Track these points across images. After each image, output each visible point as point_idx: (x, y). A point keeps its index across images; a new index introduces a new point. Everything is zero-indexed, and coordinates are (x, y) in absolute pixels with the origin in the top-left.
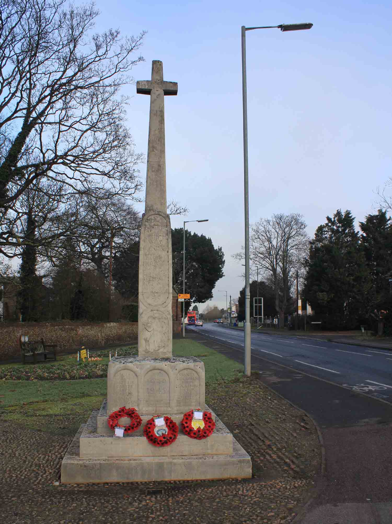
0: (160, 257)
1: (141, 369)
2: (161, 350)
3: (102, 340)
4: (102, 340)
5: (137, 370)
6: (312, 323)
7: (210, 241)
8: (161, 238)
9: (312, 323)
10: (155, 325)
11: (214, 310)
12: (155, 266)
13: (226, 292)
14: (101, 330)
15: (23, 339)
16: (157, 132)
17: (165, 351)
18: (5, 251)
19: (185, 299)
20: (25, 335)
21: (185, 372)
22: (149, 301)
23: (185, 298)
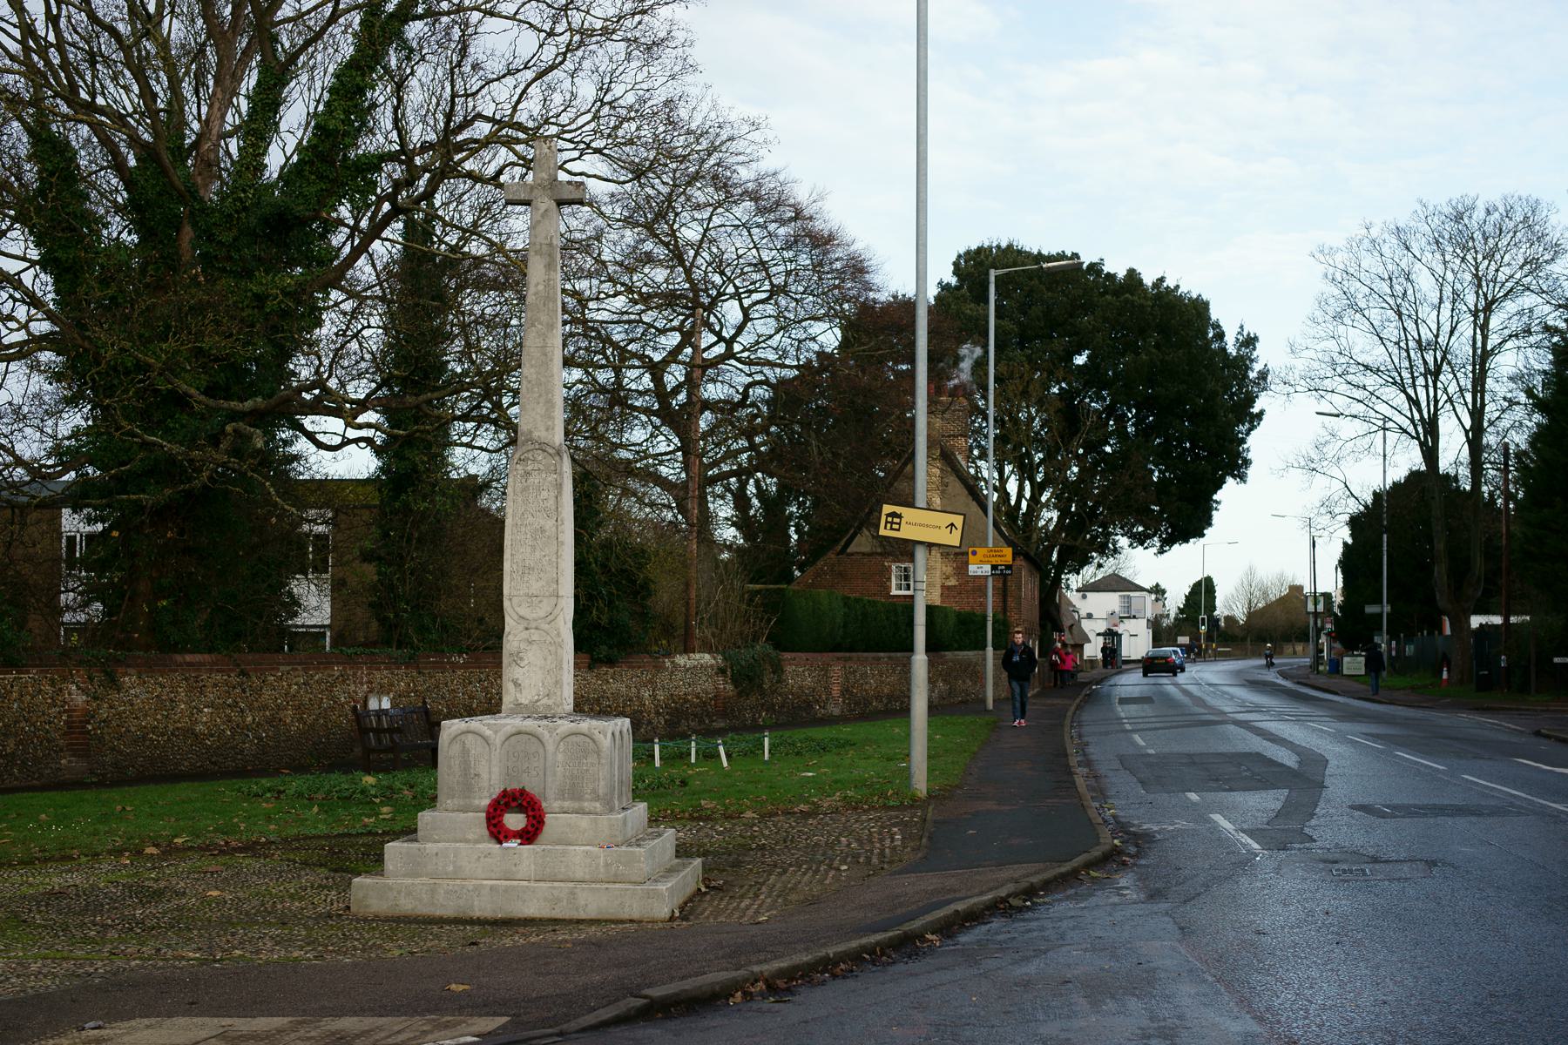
0: (543, 530)
1: (496, 732)
2: (545, 701)
3: (658, 713)
4: (658, 713)
5: (488, 733)
6: (1556, 660)
7: (1199, 308)
8: (545, 494)
9: (1556, 660)
10: (532, 656)
11: (1282, 600)
12: (533, 548)
13: (1277, 529)
14: (650, 681)
15: (373, 704)
16: (541, 287)
17: (550, 702)
18: (309, 428)
19: (994, 567)
20: (382, 691)
21: (574, 738)
22: (522, 611)
23: (995, 561)
